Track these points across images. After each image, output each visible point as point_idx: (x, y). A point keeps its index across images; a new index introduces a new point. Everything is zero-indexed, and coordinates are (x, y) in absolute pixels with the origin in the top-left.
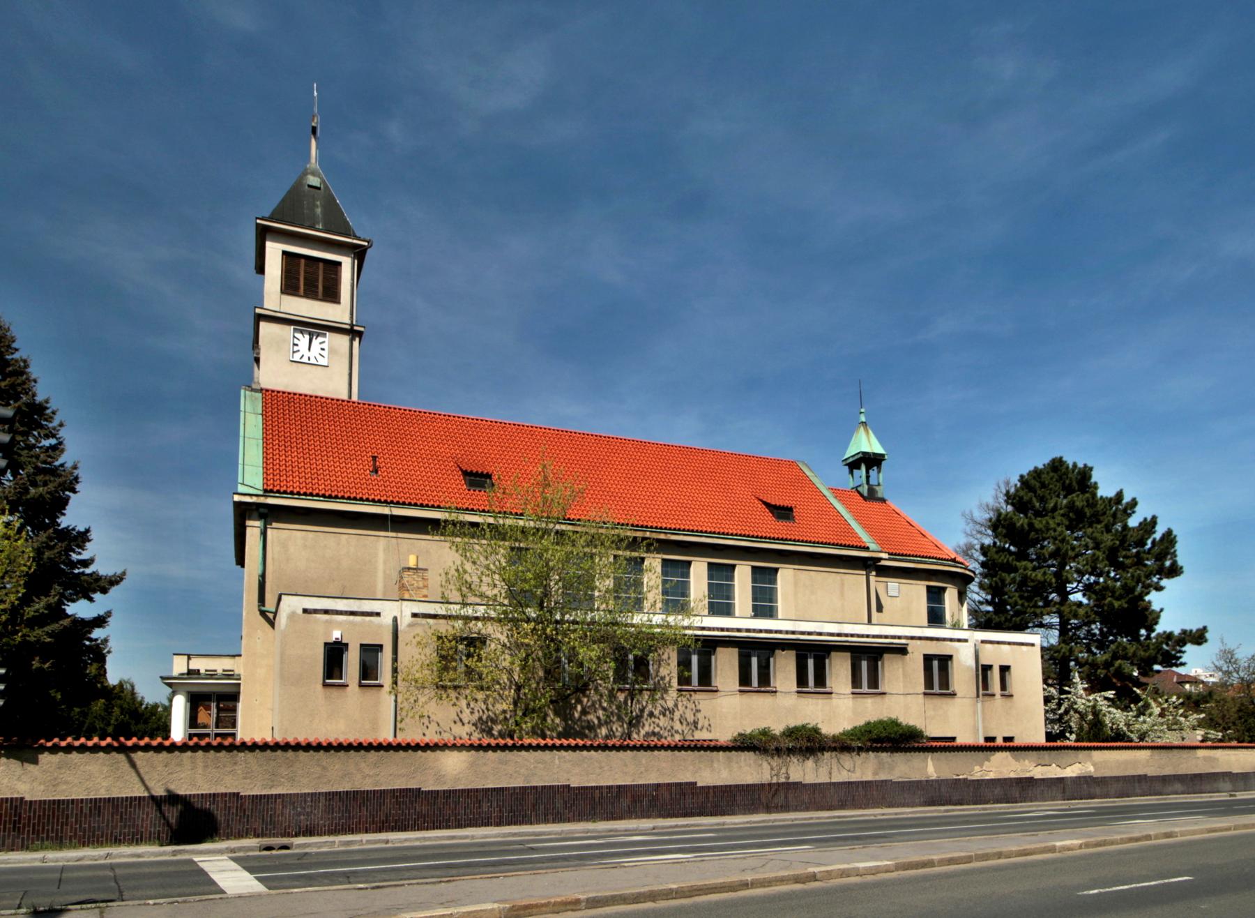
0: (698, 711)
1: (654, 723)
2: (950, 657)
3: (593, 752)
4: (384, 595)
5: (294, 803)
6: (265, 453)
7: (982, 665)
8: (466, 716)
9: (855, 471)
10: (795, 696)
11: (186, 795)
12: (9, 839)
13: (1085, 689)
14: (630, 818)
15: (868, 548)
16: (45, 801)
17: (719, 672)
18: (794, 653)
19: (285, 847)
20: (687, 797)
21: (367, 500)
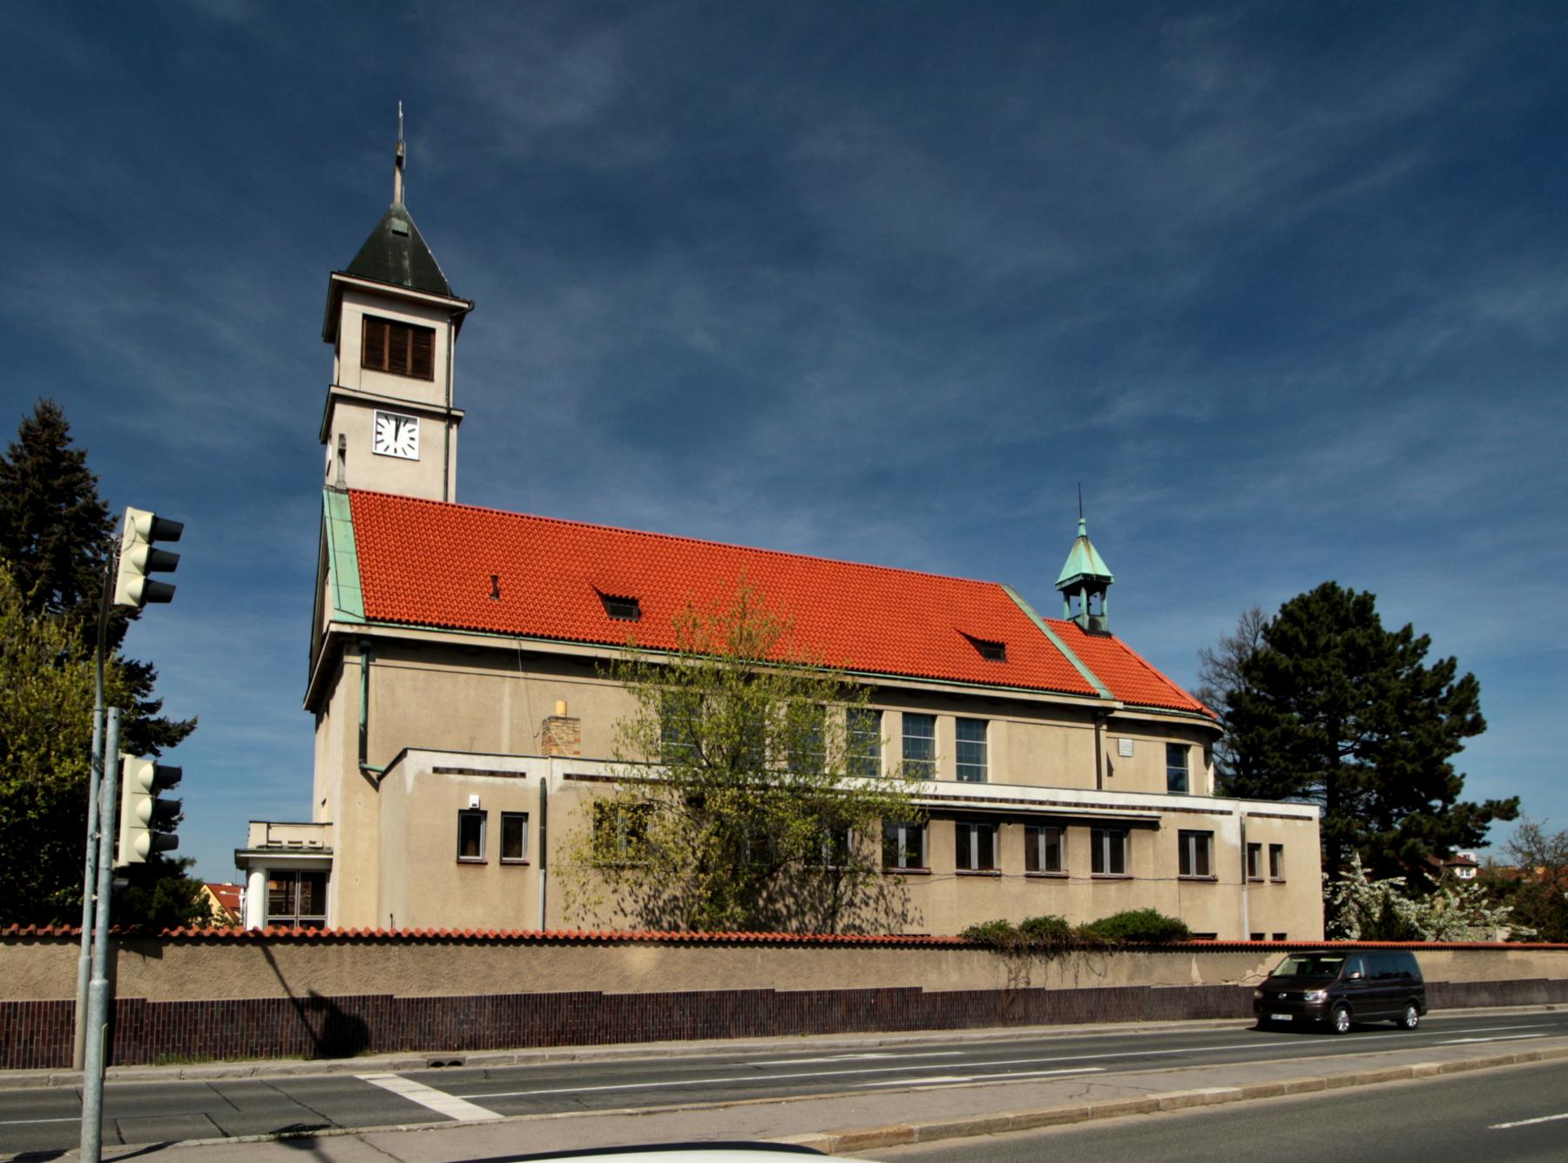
0: (908, 900)
1: (854, 913)
2: (1210, 834)
3: (801, 950)
4: (511, 749)
5: (456, 1008)
6: (362, 570)
7: (1249, 844)
8: (629, 905)
9: (1072, 598)
10: (1023, 881)
11: (332, 998)
12: (129, 1049)
13: (1366, 874)
14: (844, 1031)
15: (1098, 695)
16: (170, 1003)
17: (932, 850)
18: (1022, 827)
19: (456, 1063)
20: (910, 1006)
21: (491, 631)
